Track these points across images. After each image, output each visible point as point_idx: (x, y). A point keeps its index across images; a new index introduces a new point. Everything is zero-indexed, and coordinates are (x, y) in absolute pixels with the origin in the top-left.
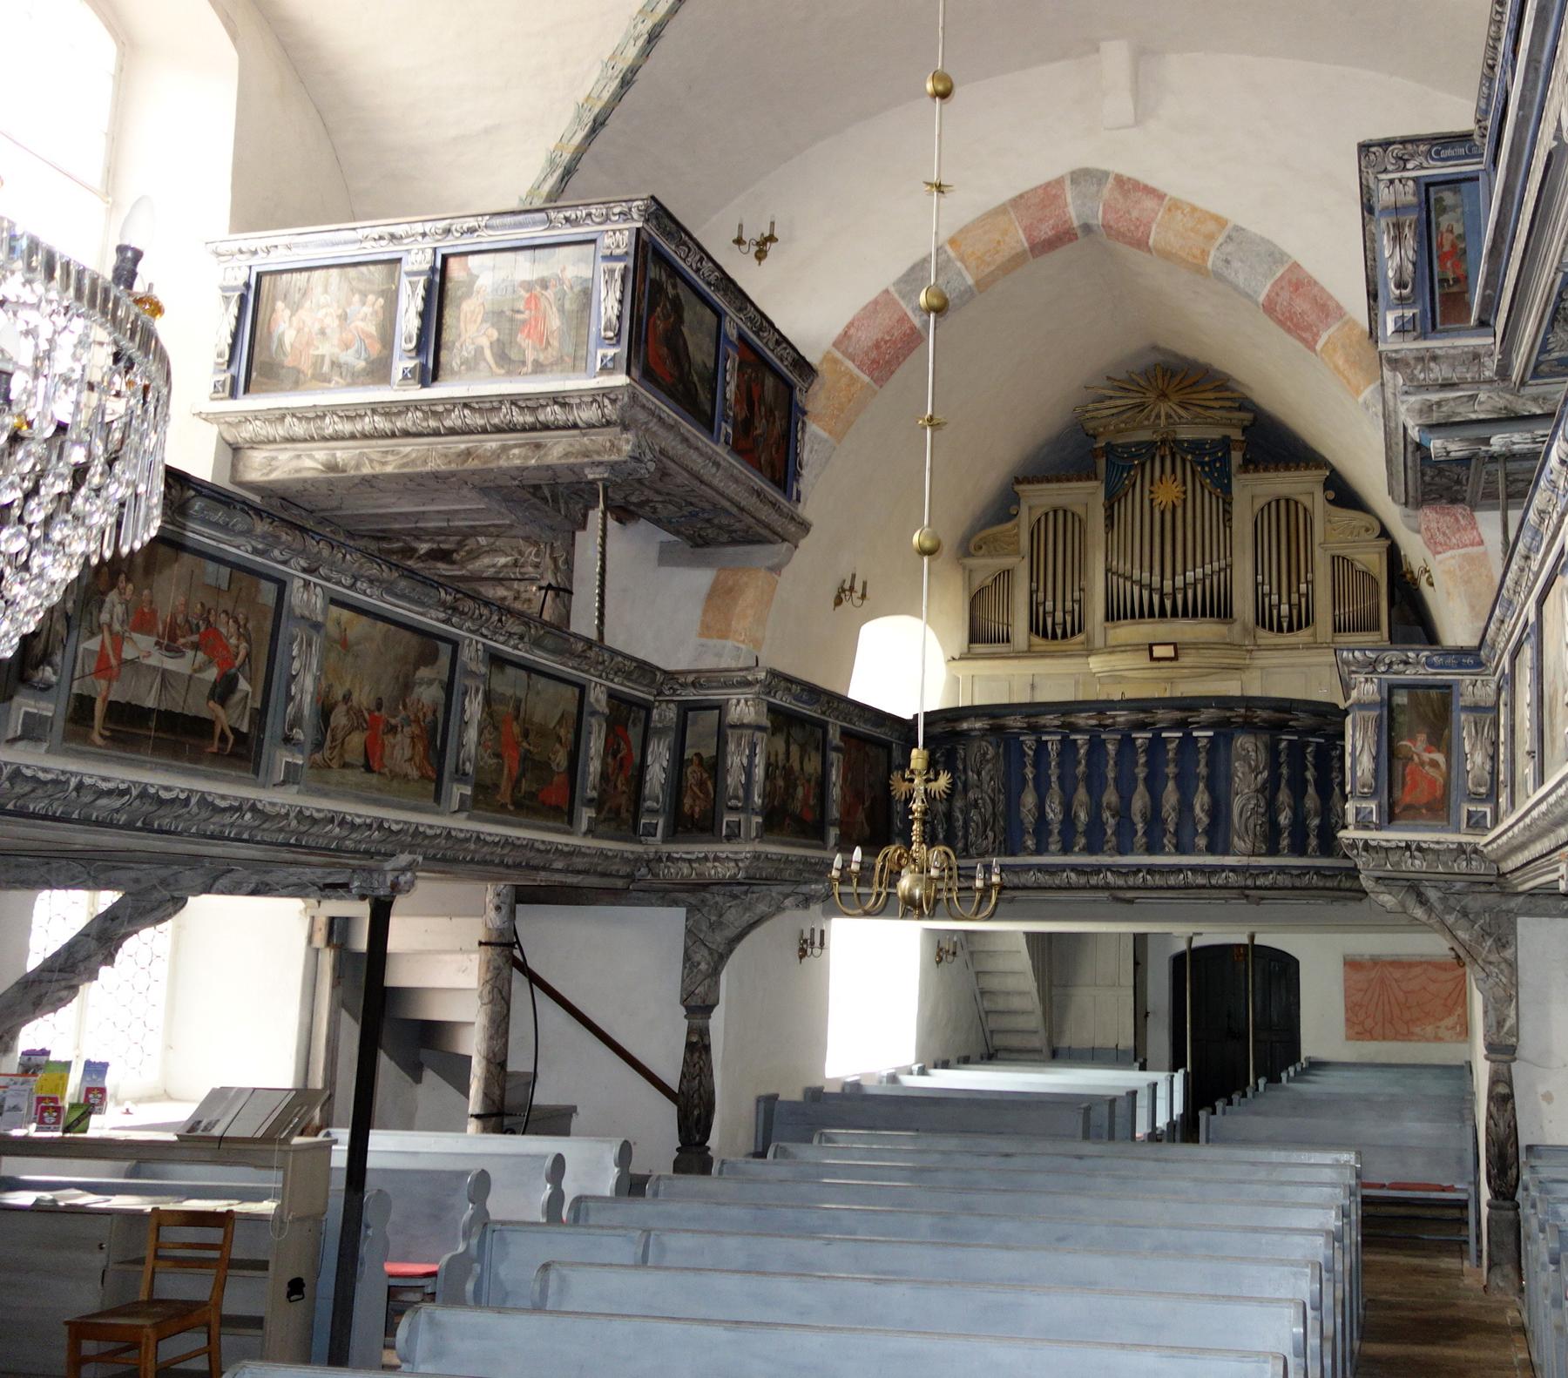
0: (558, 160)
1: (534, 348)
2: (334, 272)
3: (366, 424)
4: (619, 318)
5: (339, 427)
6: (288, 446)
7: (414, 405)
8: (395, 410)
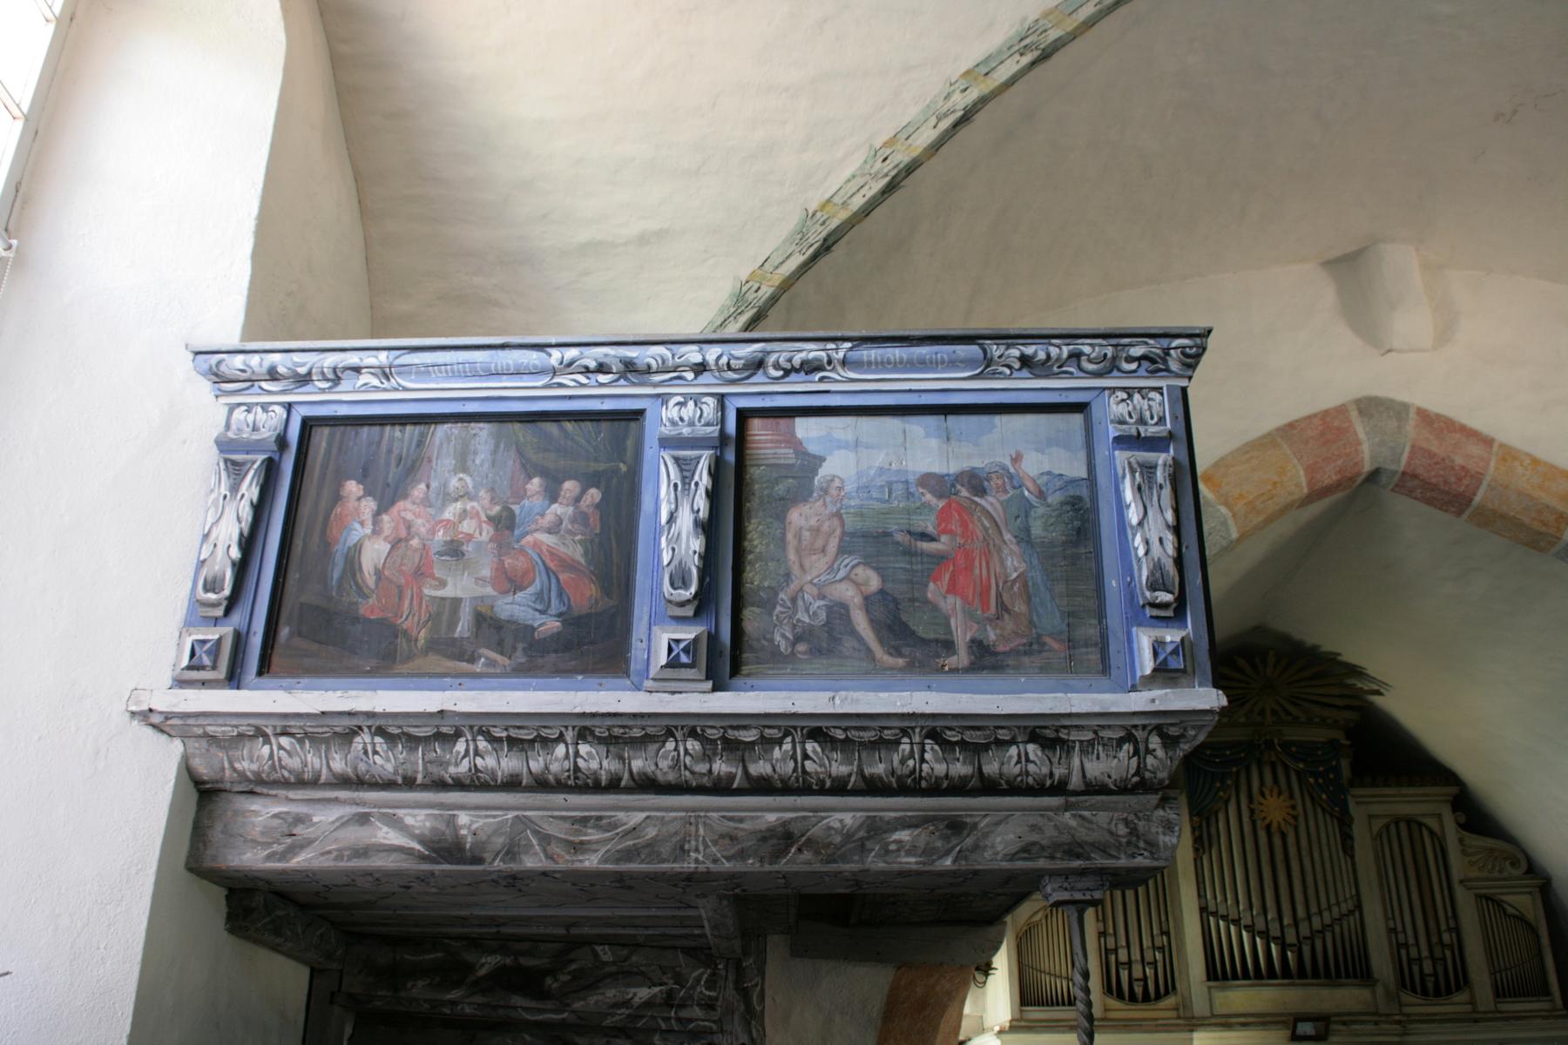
0: (751, 296)
1: (969, 615)
2: (483, 430)
3: (557, 760)
4: (1179, 561)
5: (489, 762)
6: (343, 794)
7: (692, 726)
8: (637, 733)
